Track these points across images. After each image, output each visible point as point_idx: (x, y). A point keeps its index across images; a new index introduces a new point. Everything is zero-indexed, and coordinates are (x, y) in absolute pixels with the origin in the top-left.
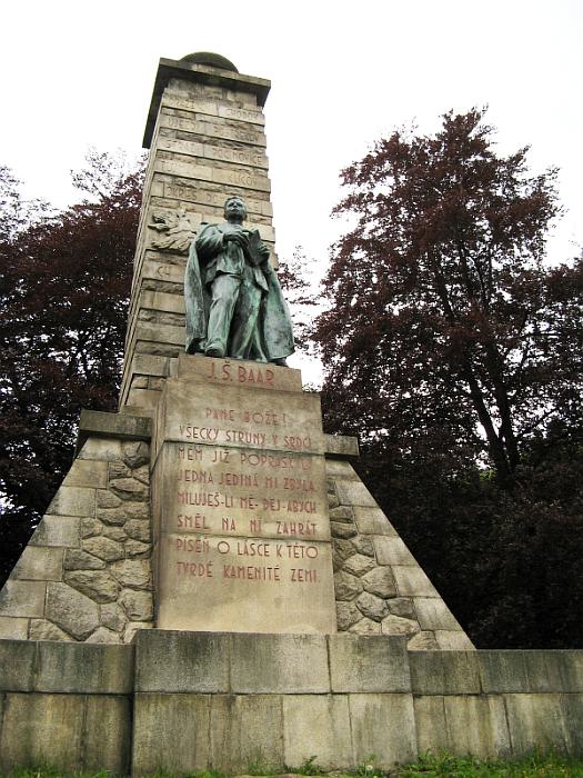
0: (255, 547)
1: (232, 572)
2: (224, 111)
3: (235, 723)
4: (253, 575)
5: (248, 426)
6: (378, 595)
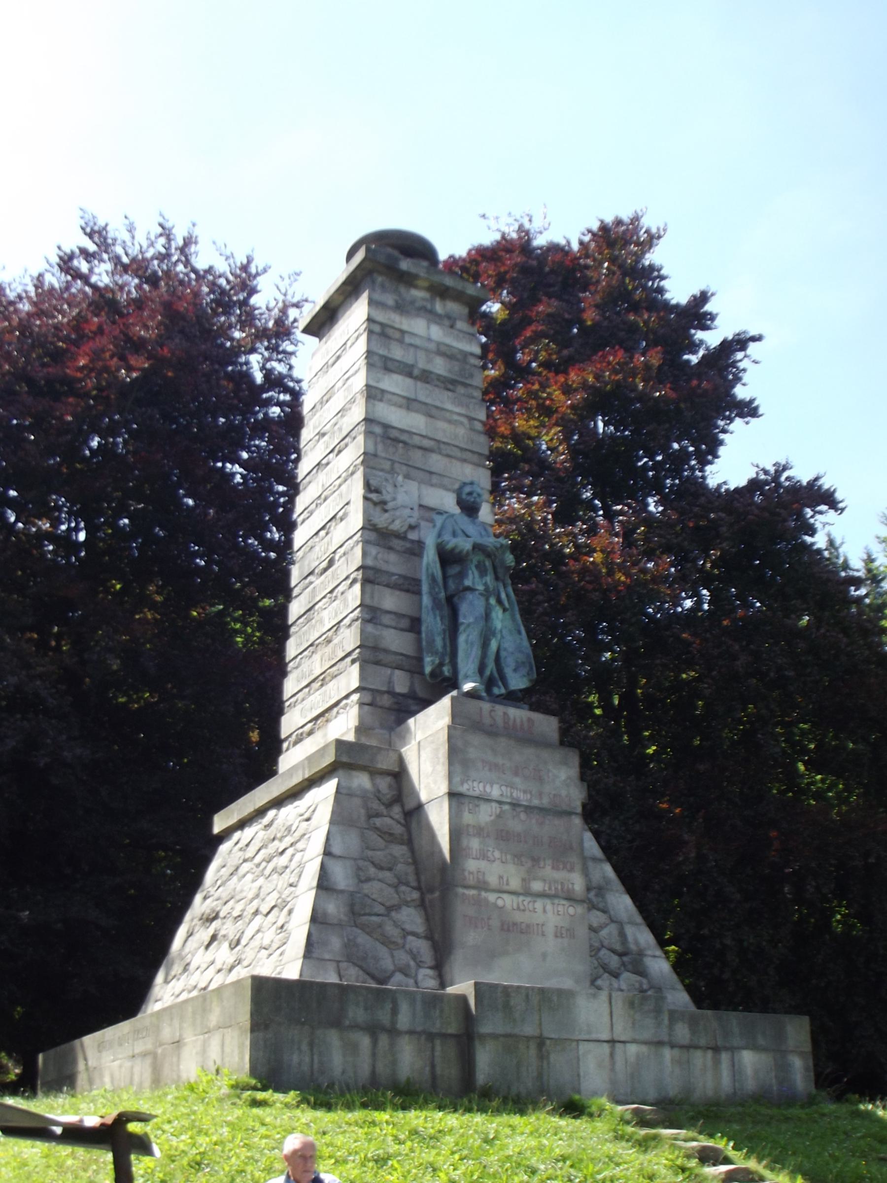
0: (526, 903)
2: (436, 332)
3: (545, 1062)
5: (517, 780)
6: (614, 951)
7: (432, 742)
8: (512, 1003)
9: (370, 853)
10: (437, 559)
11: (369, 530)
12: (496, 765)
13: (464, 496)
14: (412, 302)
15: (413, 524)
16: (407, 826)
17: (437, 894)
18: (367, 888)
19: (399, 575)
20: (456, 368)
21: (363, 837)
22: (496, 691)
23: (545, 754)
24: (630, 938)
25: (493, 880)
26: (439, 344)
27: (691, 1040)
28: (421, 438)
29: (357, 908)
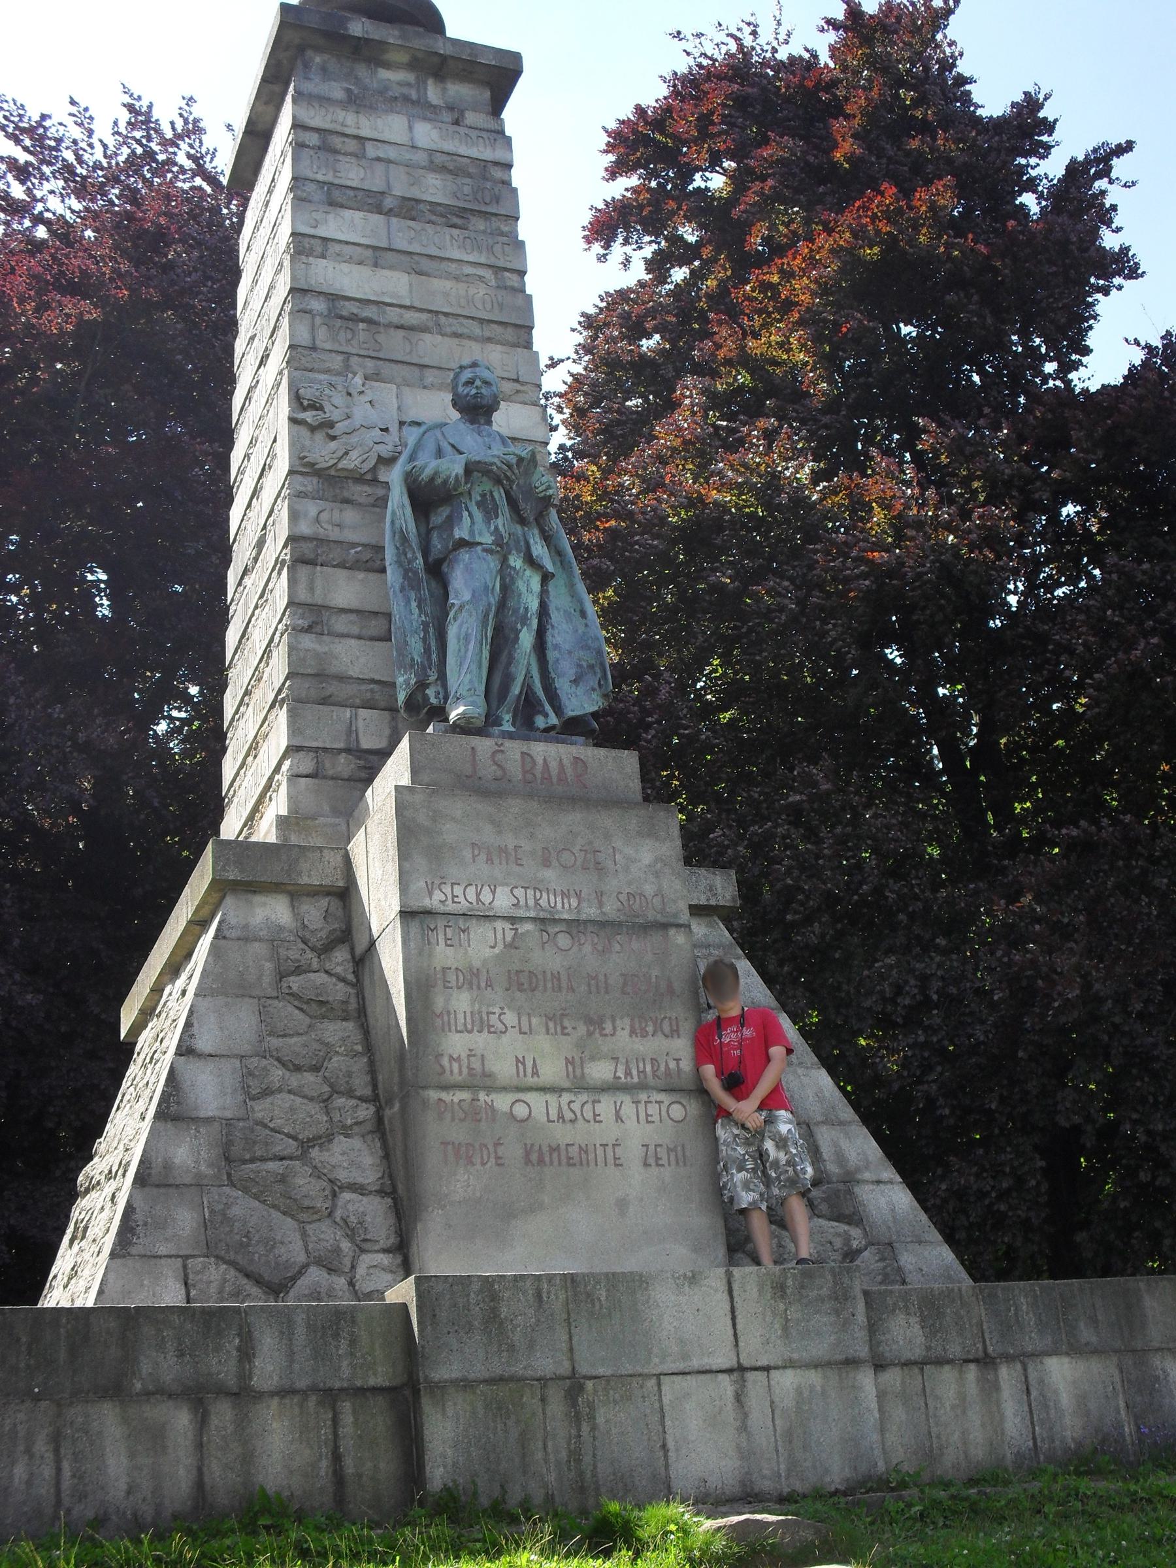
0: (576, 1106)
2: (426, 134)
3: (585, 1428)
5: (549, 874)
8: (504, 1312)
9: (275, 1042)
10: (407, 502)
11: (301, 473)
12: (503, 850)
14: (382, 91)
15: (385, 454)
17: (397, 1106)
18: (260, 1110)
19: (363, 545)
20: (467, 190)
21: (263, 1014)
23: (607, 820)
24: (826, 1151)
25: (504, 1069)
26: (431, 152)
27: (928, 1348)
28: (402, 311)
29: (236, 1150)
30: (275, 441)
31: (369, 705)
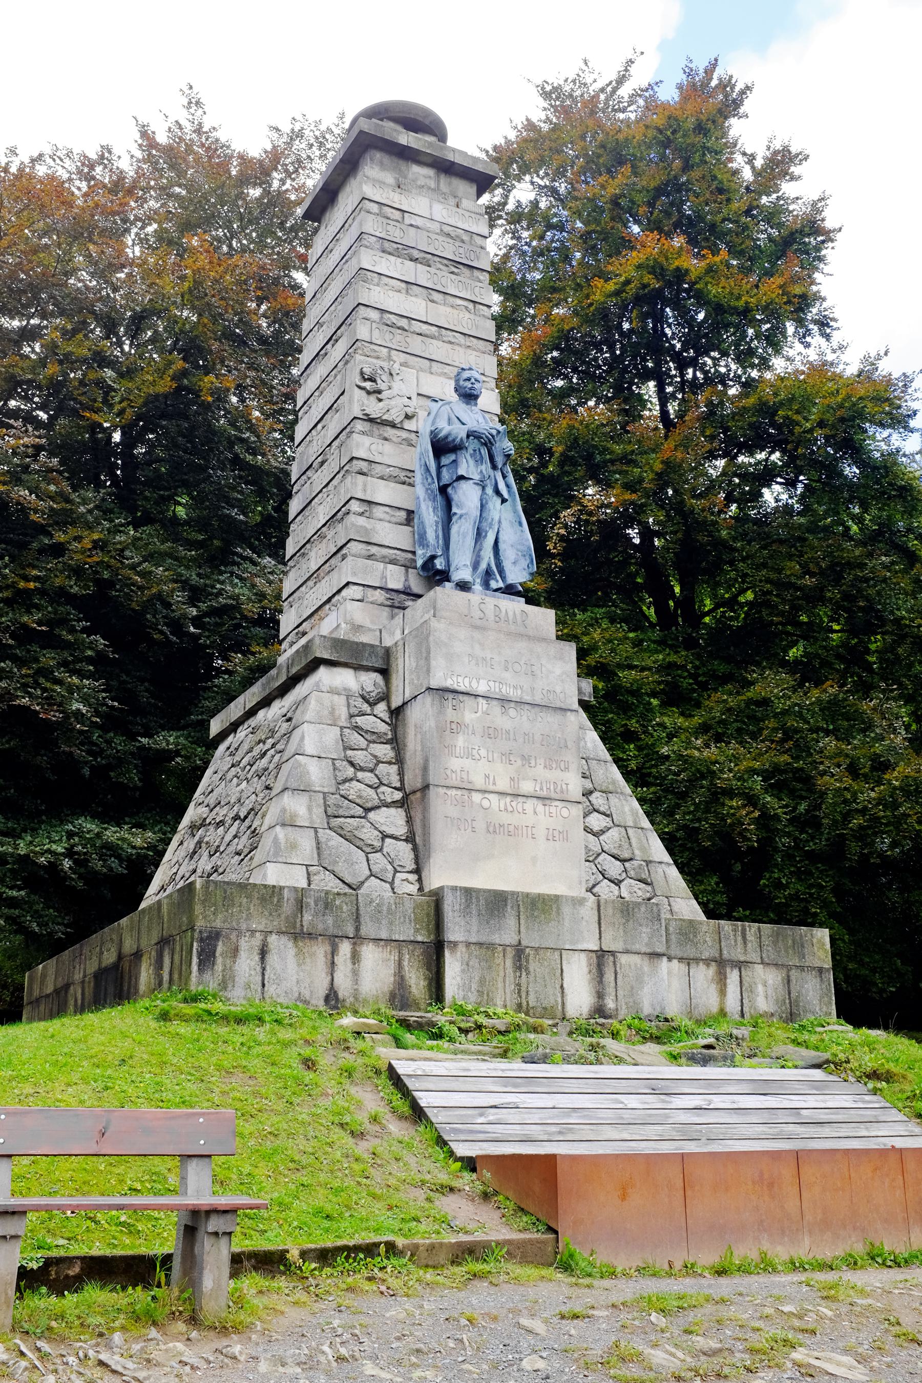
1: (493, 829)
2: (441, 212)
4: (511, 832)
5: (507, 675)
7: (416, 636)
13: (461, 383)
16: (394, 728)
22: (494, 584)
23: (539, 648)
30: (343, 393)
31: (393, 562)
